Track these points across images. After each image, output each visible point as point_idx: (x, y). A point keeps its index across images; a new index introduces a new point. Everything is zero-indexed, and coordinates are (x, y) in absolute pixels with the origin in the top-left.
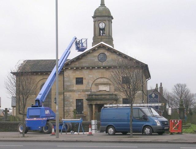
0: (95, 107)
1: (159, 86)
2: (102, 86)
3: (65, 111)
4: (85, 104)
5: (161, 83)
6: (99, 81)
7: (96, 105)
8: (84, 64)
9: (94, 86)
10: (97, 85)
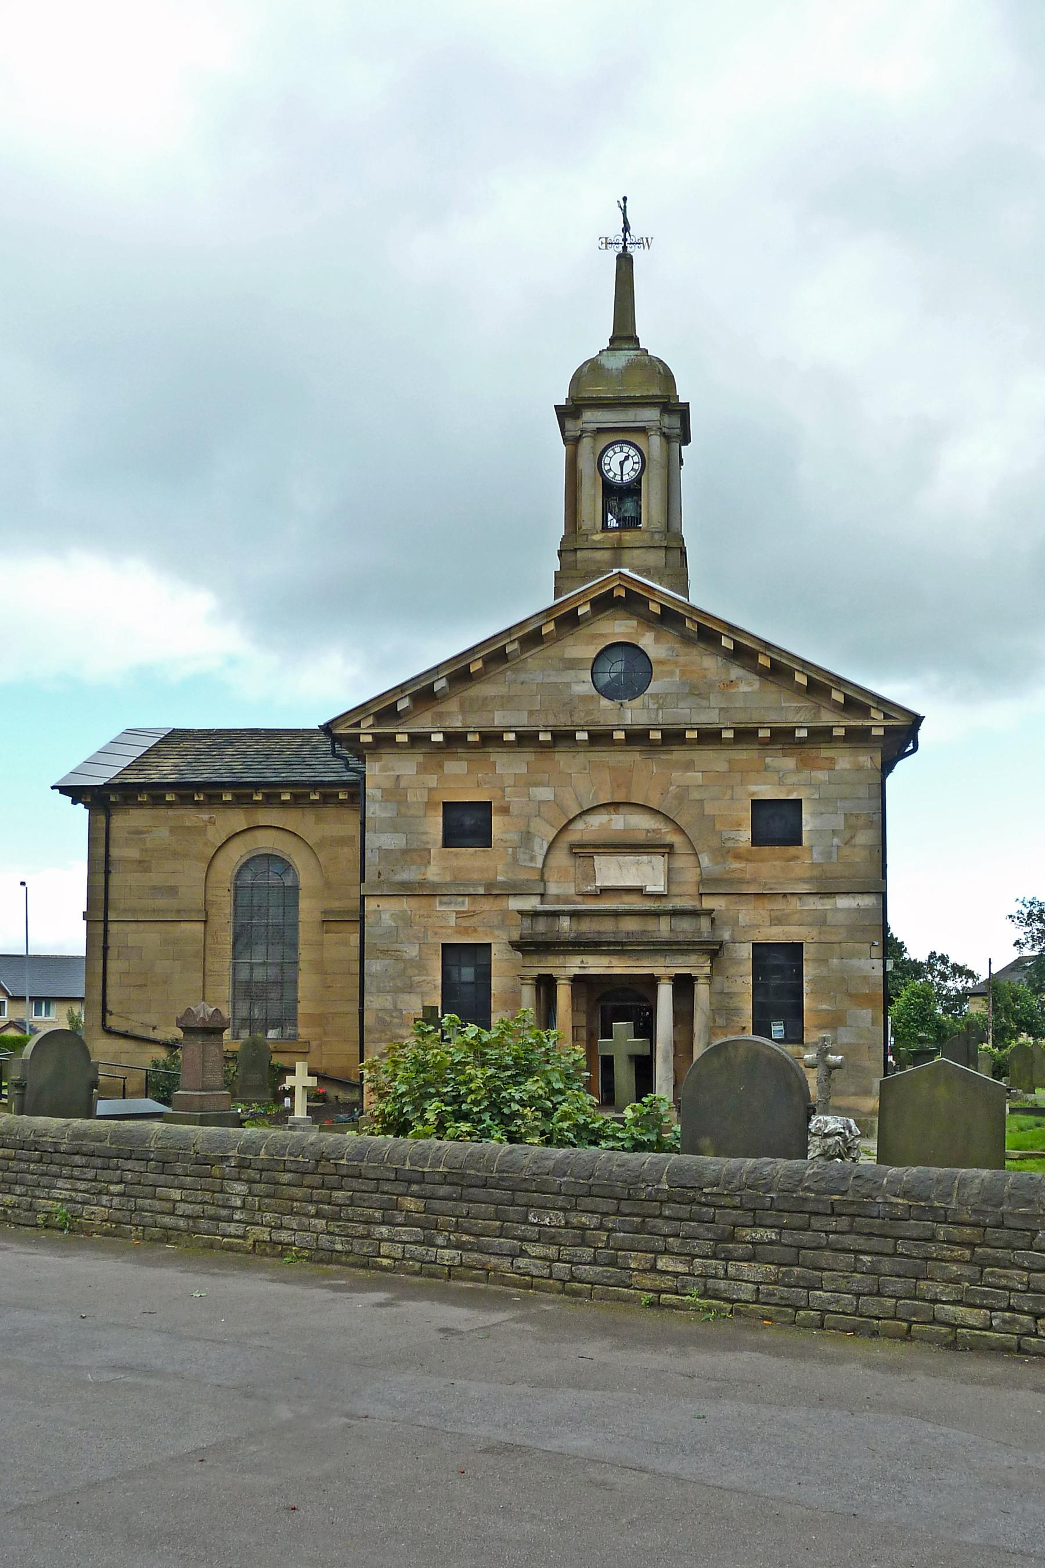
0: (574, 996)
2: (620, 858)
3: (369, 1019)
4: (503, 966)
7: (577, 981)
9: (561, 858)
10: (585, 851)
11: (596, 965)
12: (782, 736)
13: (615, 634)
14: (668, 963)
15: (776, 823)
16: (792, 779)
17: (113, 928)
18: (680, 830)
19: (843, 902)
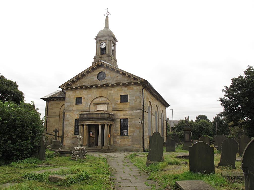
1: (187, 118)
2: (100, 105)
5: (188, 116)
8: (84, 84)
11: (90, 122)
12: (124, 84)
13: (101, 70)
14: (100, 122)
17: (48, 118)
18: (109, 101)
19: (135, 111)
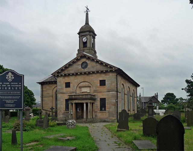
1: (156, 94)
6: (80, 85)
7: (76, 103)
9: (78, 88)
10: (80, 87)
11: (77, 101)
15: (103, 83)
16: (105, 77)
